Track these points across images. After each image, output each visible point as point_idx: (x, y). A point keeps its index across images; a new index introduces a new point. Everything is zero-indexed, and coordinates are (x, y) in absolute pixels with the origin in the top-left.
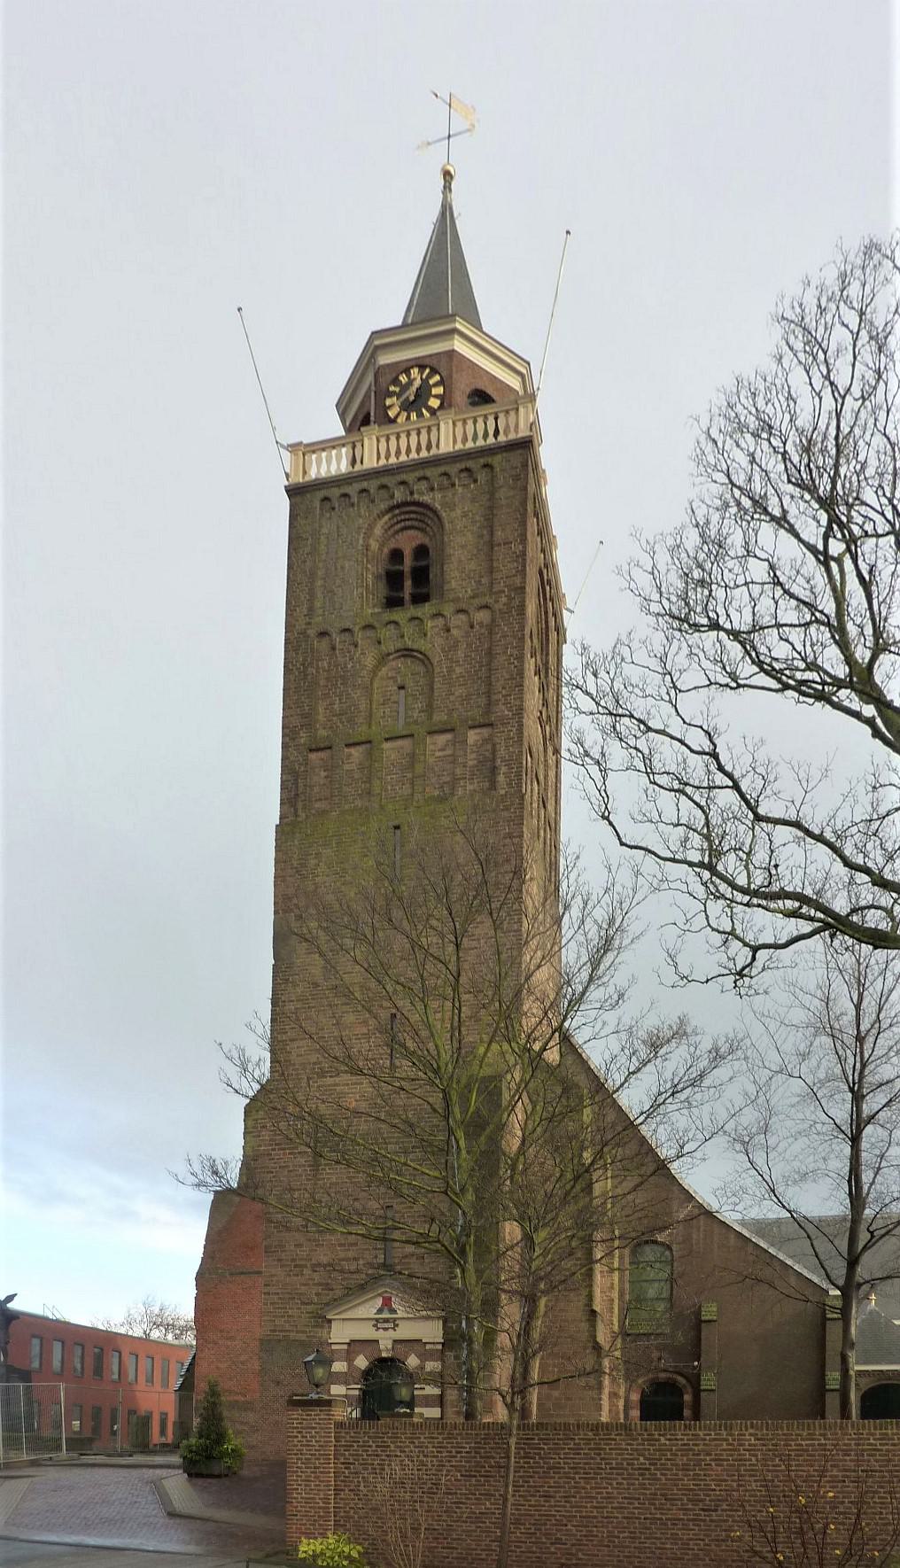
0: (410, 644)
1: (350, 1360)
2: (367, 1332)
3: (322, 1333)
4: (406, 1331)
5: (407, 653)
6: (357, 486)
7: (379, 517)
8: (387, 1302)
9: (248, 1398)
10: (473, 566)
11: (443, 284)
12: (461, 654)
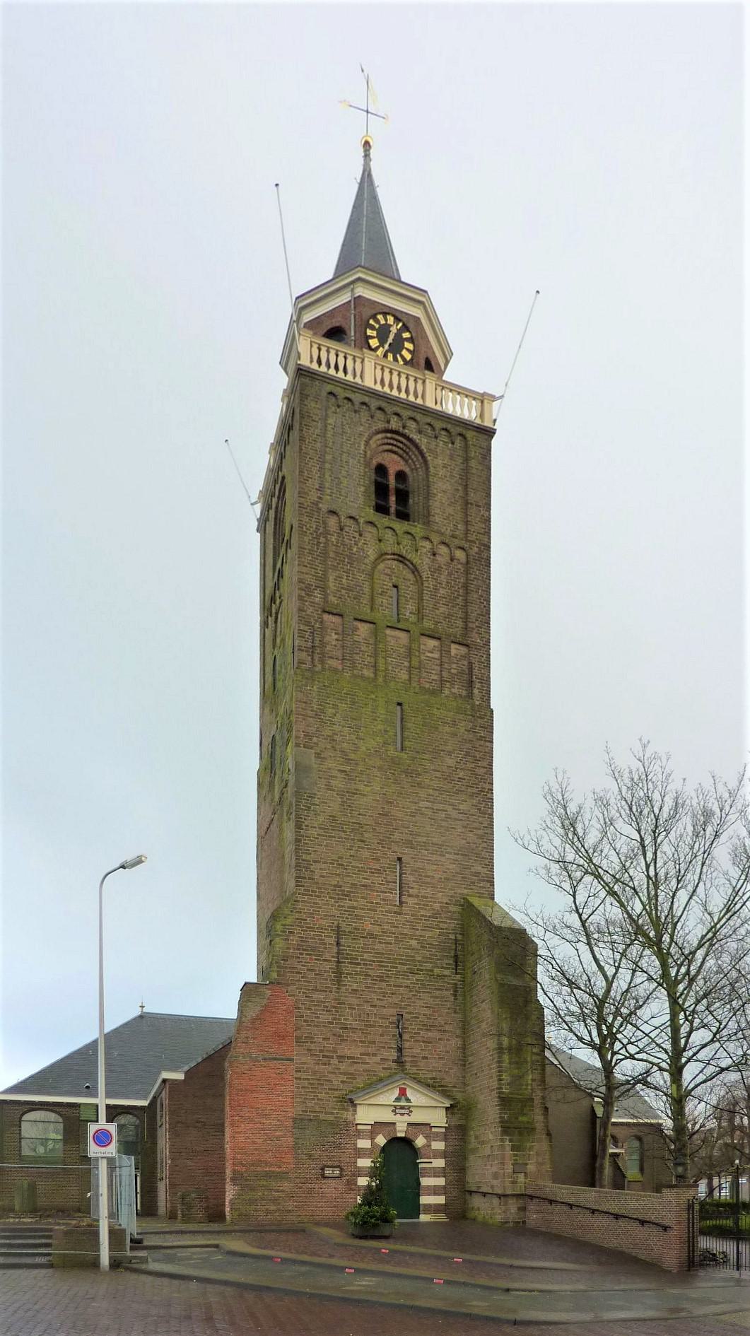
0: (404, 553)
1: (372, 1139)
2: (387, 1116)
3: (348, 1115)
4: (417, 1117)
5: (401, 559)
6: (459, 430)
7: (378, 432)
8: (403, 1092)
9: (284, 1169)
10: (450, 510)
11: (366, 242)
12: (443, 578)
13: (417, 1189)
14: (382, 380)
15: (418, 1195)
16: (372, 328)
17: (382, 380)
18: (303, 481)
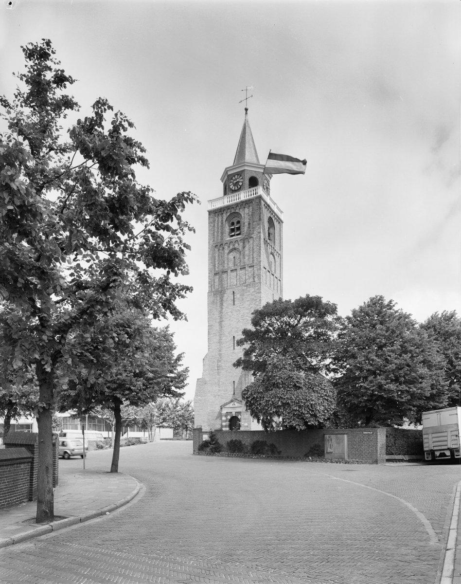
2: (230, 410)
4: (238, 410)
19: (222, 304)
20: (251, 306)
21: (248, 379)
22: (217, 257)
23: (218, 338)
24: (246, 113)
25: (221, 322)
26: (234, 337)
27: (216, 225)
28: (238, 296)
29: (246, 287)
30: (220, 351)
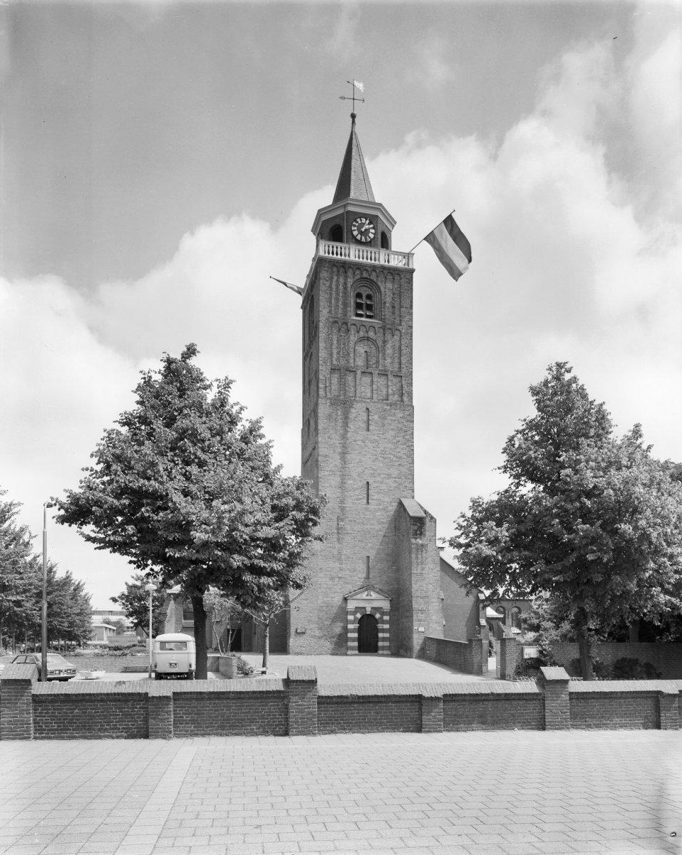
2: (362, 604)
4: (376, 604)
13: (377, 639)
14: (367, 257)
15: (377, 641)
16: (355, 226)
17: (367, 257)
18: (345, 288)
19: (346, 425)
20: (398, 439)
21: (422, 557)
22: (335, 342)
23: (339, 479)
24: (353, 122)
25: (343, 454)
26: (368, 483)
27: (334, 286)
28: (376, 417)
29: (389, 407)
30: (342, 502)
